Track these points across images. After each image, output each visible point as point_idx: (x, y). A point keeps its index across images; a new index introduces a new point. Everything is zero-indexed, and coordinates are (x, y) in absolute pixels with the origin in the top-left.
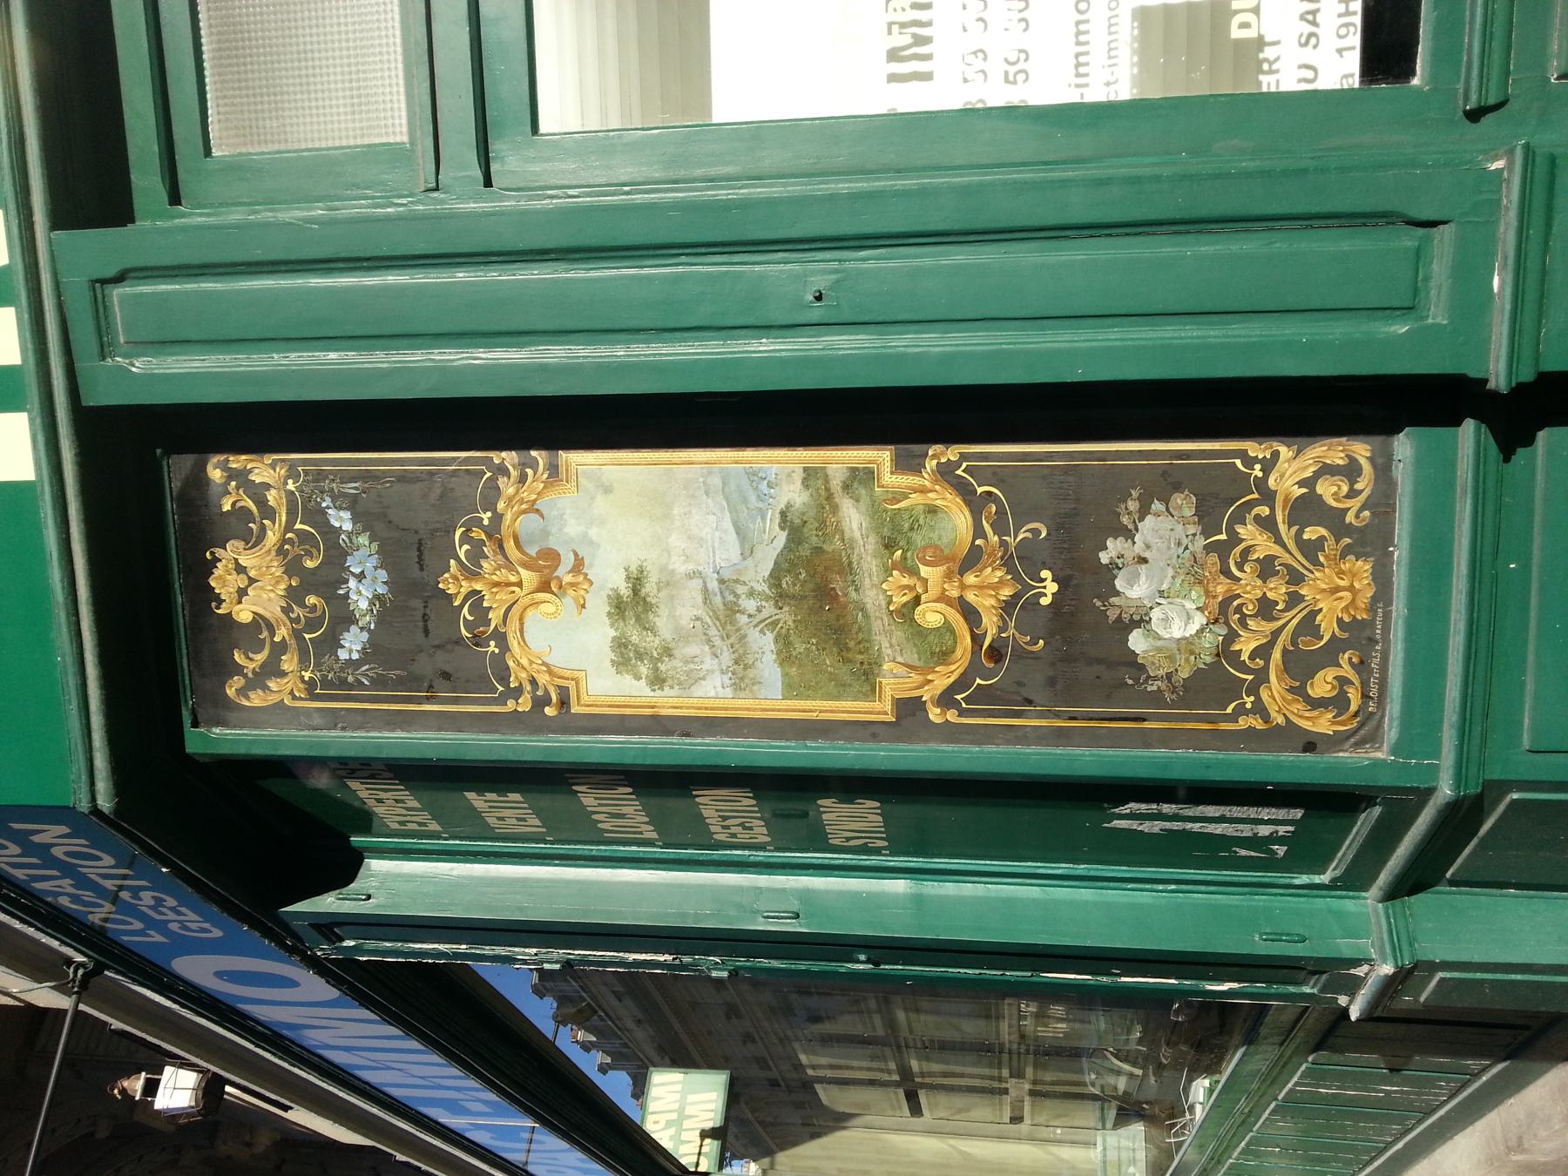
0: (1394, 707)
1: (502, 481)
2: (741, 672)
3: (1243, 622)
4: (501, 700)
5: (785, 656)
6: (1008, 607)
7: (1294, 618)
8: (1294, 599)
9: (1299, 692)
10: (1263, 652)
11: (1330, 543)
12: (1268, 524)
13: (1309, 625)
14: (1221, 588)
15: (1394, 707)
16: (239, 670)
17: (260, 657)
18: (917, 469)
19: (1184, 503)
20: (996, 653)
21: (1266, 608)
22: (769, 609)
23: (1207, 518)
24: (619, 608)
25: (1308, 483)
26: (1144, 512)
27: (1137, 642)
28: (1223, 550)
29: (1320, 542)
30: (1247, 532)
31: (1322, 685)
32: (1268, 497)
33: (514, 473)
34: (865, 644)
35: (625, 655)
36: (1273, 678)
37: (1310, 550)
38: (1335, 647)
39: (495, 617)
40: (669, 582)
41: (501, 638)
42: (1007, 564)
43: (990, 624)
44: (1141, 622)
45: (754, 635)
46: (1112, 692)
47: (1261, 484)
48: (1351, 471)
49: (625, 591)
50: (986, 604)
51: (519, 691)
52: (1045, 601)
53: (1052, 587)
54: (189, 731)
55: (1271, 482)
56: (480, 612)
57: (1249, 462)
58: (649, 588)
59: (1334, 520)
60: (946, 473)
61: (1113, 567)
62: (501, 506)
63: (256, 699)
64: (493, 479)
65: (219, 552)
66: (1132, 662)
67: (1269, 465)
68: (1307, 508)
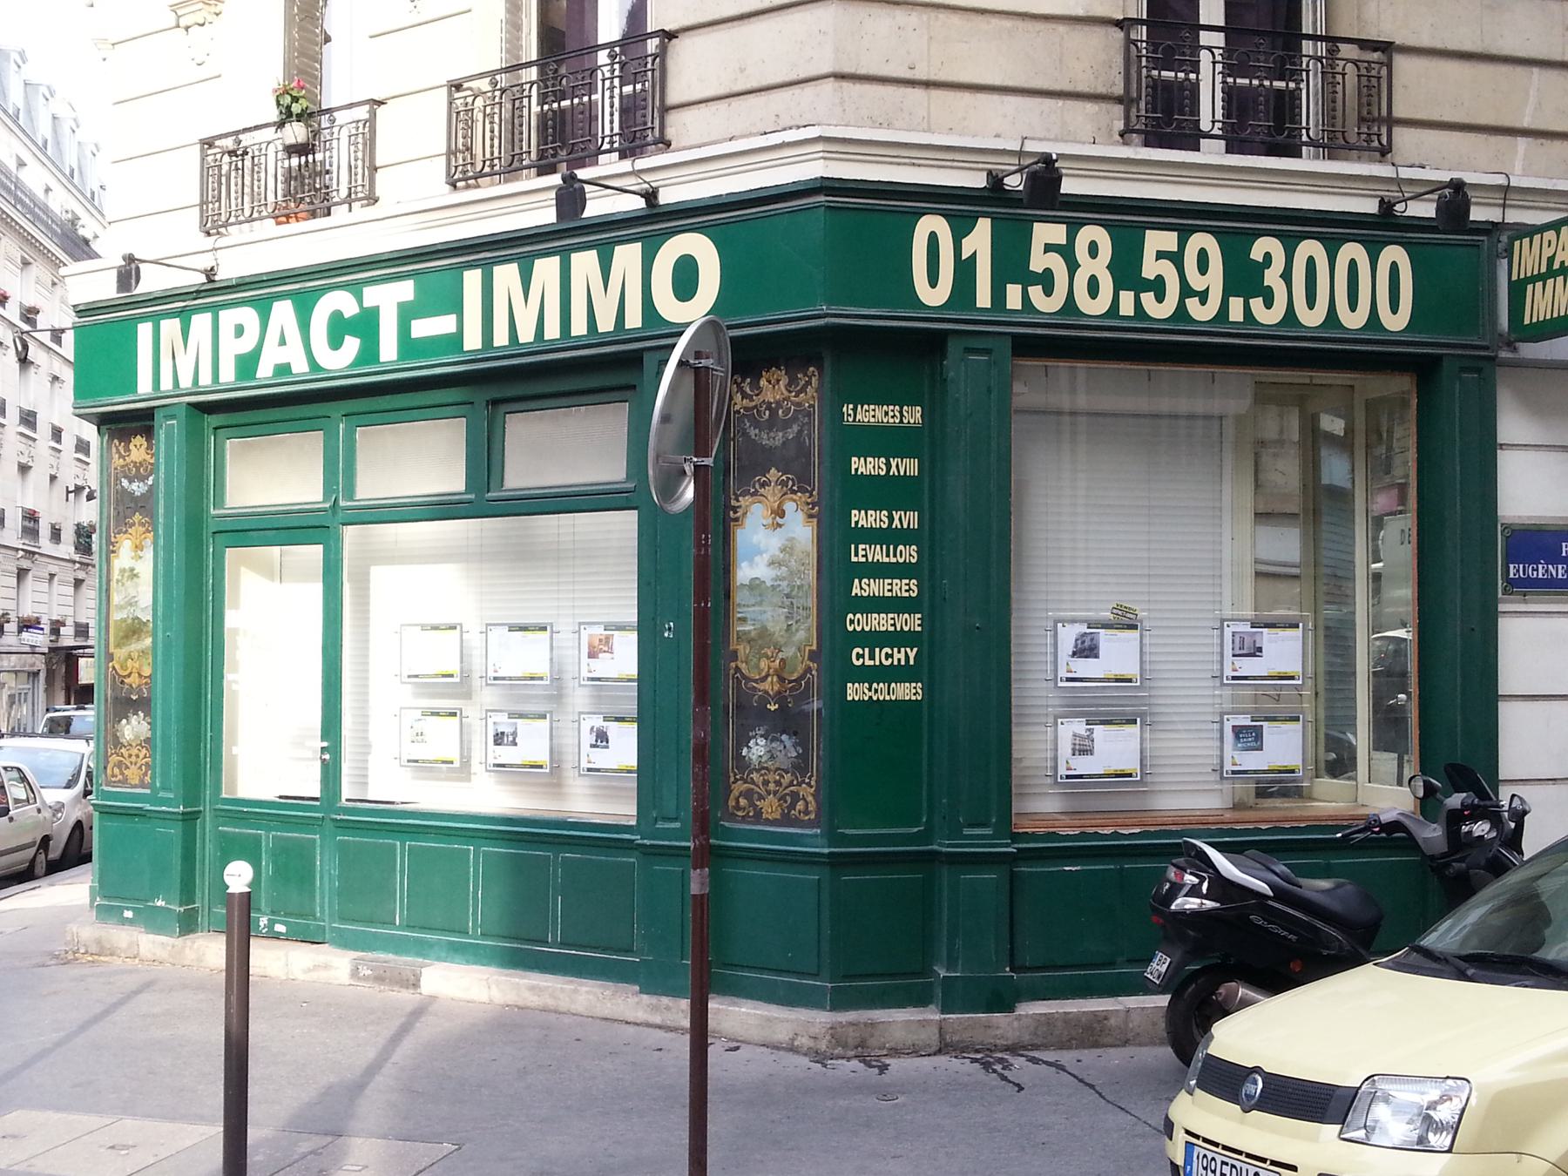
0: (110, 789)
1: (807, 494)
2: (120, 608)
3: (762, 775)
4: (735, 494)
5: (124, 620)
6: (766, 692)
7: (763, 793)
8: (769, 793)
9: (741, 794)
10: (753, 782)
11: (785, 805)
12: (791, 784)
13: (761, 798)
14: (134, 744)
15: (110, 789)
16: (743, 381)
17: (748, 390)
18: (810, 659)
19: (149, 735)
20: (122, 682)
21: (766, 783)
22: (131, 616)
23: (147, 740)
24: (132, 570)
25: (804, 799)
26: (149, 723)
27: (124, 721)
28: (140, 745)
29: (786, 802)
30: (144, 751)
31: (743, 802)
32: (799, 784)
33: (809, 500)
34: (124, 644)
35: (123, 571)
36: (746, 785)
37: (140, 768)
38: (122, 774)
39: (130, 530)
40: (137, 585)
41: (126, 532)
42: (779, 692)
43: (761, 686)
44: (128, 723)
45: (126, 611)
46: (115, 717)
47: (803, 782)
48: (807, 812)
49: (135, 572)
50: (766, 686)
51: (738, 501)
52: (768, 706)
53: (773, 708)
54: (105, 427)
55: (804, 785)
56: (763, 485)
57: (810, 778)
58: (135, 579)
59: (792, 806)
60: (809, 670)
61: (137, 715)
62: (799, 494)
63: (114, 450)
64: (808, 491)
65: (783, 372)
66: (120, 721)
67: (809, 784)
68: (795, 797)
